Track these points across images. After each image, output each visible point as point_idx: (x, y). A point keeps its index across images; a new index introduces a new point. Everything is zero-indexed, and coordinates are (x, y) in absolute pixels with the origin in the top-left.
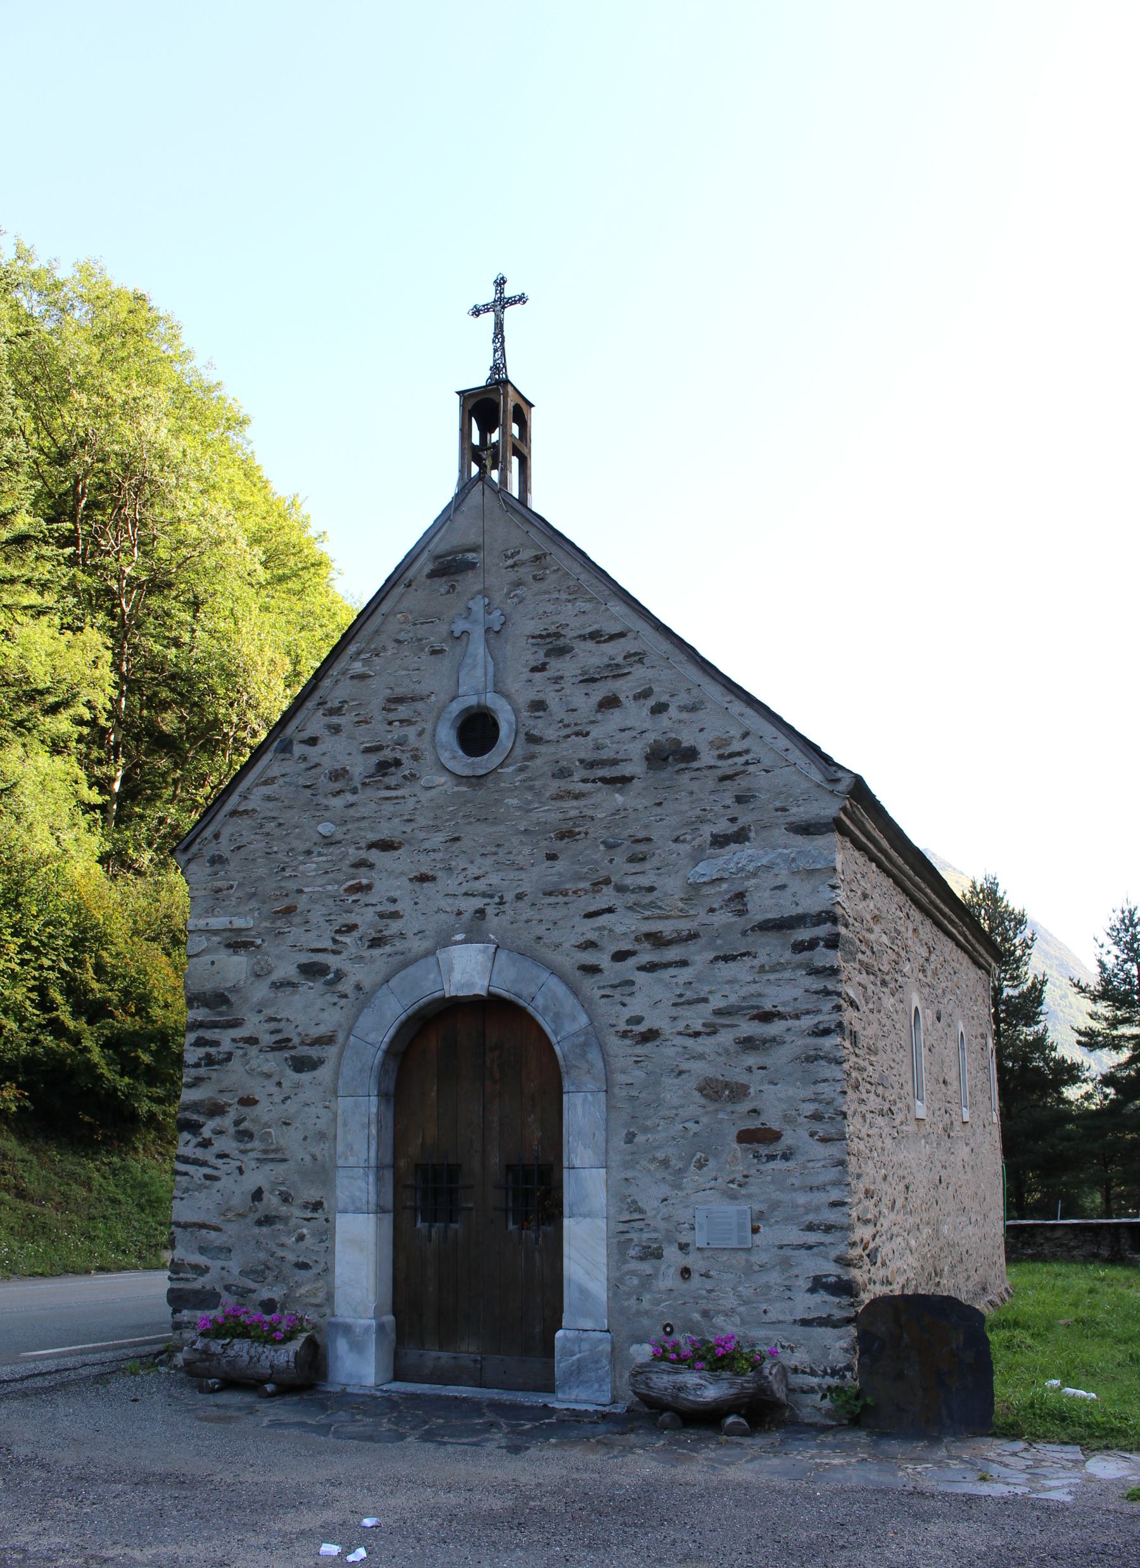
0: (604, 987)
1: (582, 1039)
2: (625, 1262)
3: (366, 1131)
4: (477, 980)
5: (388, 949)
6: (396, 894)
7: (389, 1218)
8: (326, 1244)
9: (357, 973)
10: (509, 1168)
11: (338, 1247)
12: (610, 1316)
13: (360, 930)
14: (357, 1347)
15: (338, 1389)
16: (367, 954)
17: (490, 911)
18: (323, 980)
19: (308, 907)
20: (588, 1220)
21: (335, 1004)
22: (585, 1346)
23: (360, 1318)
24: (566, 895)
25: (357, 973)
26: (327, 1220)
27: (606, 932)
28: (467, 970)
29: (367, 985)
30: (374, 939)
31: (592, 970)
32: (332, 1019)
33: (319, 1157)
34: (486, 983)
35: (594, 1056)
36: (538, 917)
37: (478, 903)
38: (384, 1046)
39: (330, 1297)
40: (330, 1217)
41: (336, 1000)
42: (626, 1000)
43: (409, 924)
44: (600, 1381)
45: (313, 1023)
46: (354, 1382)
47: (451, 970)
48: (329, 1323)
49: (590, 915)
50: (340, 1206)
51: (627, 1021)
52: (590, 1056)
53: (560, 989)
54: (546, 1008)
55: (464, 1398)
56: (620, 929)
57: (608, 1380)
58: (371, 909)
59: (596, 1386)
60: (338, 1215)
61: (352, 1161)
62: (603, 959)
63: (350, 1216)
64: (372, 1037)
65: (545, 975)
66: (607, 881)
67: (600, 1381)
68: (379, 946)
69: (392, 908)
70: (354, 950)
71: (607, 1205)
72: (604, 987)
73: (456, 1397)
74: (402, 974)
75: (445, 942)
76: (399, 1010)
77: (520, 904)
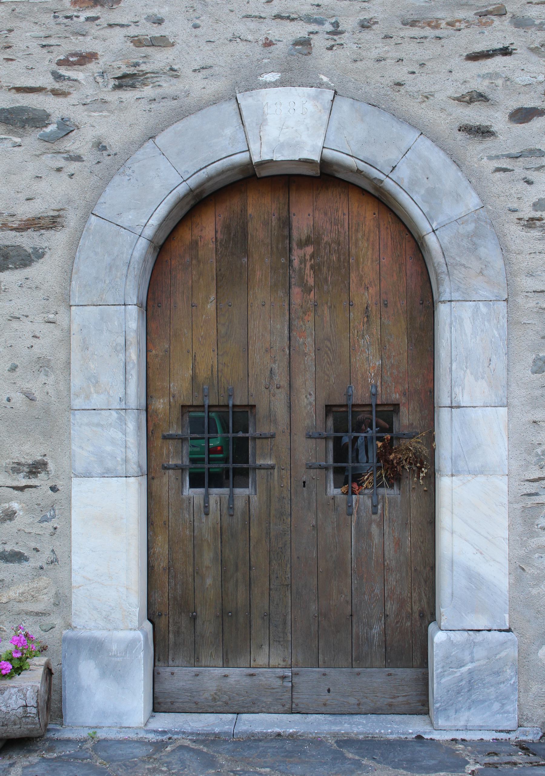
0: (497, 157)
1: (471, 227)
2: (532, 535)
3: (122, 356)
4: (304, 138)
5: (148, 91)
6: (164, 11)
7: (144, 480)
8: (54, 523)
9: (94, 126)
10: (329, 409)
11: (76, 527)
12: (512, 610)
13: (101, 61)
14: (113, 671)
15: (84, 734)
16: (114, 97)
17: (319, 42)
18: (39, 133)
19: (9, 26)
20: (481, 479)
21: (59, 170)
22: (480, 653)
23: (115, 629)
24: (437, 27)
25: (94, 126)
26: (54, 489)
27: (500, 82)
28: (289, 125)
29: (115, 141)
30: (125, 76)
31: (483, 132)
32: (52, 193)
33: (37, 395)
34: (320, 144)
35: (489, 250)
36: (398, 55)
37: (300, 30)
38: (149, 232)
39: (62, 601)
40: (60, 484)
41: (61, 163)
42: (532, 175)
43: (188, 52)
44: (502, 699)
45: (22, 197)
46: (108, 722)
47: (262, 123)
48: (64, 640)
49: (474, 57)
50: (79, 467)
51: (534, 205)
52: (482, 251)
53: (437, 158)
54: (414, 182)
55: (291, 735)
56: (521, 78)
57: (514, 697)
58: (119, 34)
59: (496, 706)
60: (75, 481)
61: (97, 400)
62: (497, 119)
63: (96, 483)
64: (128, 218)
65: (411, 136)
66: (500, 12)
67: (502, 699)
68: (133, 86)
69: (155, 31)
70: (90, 92)
71: (509, 458)
72: (497, 157)
73: (279, 735)
74: (179, 126)
75: (252, 85)
76: (175, 179)
77: (367, 35)
